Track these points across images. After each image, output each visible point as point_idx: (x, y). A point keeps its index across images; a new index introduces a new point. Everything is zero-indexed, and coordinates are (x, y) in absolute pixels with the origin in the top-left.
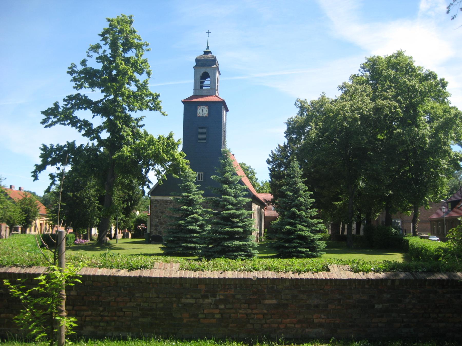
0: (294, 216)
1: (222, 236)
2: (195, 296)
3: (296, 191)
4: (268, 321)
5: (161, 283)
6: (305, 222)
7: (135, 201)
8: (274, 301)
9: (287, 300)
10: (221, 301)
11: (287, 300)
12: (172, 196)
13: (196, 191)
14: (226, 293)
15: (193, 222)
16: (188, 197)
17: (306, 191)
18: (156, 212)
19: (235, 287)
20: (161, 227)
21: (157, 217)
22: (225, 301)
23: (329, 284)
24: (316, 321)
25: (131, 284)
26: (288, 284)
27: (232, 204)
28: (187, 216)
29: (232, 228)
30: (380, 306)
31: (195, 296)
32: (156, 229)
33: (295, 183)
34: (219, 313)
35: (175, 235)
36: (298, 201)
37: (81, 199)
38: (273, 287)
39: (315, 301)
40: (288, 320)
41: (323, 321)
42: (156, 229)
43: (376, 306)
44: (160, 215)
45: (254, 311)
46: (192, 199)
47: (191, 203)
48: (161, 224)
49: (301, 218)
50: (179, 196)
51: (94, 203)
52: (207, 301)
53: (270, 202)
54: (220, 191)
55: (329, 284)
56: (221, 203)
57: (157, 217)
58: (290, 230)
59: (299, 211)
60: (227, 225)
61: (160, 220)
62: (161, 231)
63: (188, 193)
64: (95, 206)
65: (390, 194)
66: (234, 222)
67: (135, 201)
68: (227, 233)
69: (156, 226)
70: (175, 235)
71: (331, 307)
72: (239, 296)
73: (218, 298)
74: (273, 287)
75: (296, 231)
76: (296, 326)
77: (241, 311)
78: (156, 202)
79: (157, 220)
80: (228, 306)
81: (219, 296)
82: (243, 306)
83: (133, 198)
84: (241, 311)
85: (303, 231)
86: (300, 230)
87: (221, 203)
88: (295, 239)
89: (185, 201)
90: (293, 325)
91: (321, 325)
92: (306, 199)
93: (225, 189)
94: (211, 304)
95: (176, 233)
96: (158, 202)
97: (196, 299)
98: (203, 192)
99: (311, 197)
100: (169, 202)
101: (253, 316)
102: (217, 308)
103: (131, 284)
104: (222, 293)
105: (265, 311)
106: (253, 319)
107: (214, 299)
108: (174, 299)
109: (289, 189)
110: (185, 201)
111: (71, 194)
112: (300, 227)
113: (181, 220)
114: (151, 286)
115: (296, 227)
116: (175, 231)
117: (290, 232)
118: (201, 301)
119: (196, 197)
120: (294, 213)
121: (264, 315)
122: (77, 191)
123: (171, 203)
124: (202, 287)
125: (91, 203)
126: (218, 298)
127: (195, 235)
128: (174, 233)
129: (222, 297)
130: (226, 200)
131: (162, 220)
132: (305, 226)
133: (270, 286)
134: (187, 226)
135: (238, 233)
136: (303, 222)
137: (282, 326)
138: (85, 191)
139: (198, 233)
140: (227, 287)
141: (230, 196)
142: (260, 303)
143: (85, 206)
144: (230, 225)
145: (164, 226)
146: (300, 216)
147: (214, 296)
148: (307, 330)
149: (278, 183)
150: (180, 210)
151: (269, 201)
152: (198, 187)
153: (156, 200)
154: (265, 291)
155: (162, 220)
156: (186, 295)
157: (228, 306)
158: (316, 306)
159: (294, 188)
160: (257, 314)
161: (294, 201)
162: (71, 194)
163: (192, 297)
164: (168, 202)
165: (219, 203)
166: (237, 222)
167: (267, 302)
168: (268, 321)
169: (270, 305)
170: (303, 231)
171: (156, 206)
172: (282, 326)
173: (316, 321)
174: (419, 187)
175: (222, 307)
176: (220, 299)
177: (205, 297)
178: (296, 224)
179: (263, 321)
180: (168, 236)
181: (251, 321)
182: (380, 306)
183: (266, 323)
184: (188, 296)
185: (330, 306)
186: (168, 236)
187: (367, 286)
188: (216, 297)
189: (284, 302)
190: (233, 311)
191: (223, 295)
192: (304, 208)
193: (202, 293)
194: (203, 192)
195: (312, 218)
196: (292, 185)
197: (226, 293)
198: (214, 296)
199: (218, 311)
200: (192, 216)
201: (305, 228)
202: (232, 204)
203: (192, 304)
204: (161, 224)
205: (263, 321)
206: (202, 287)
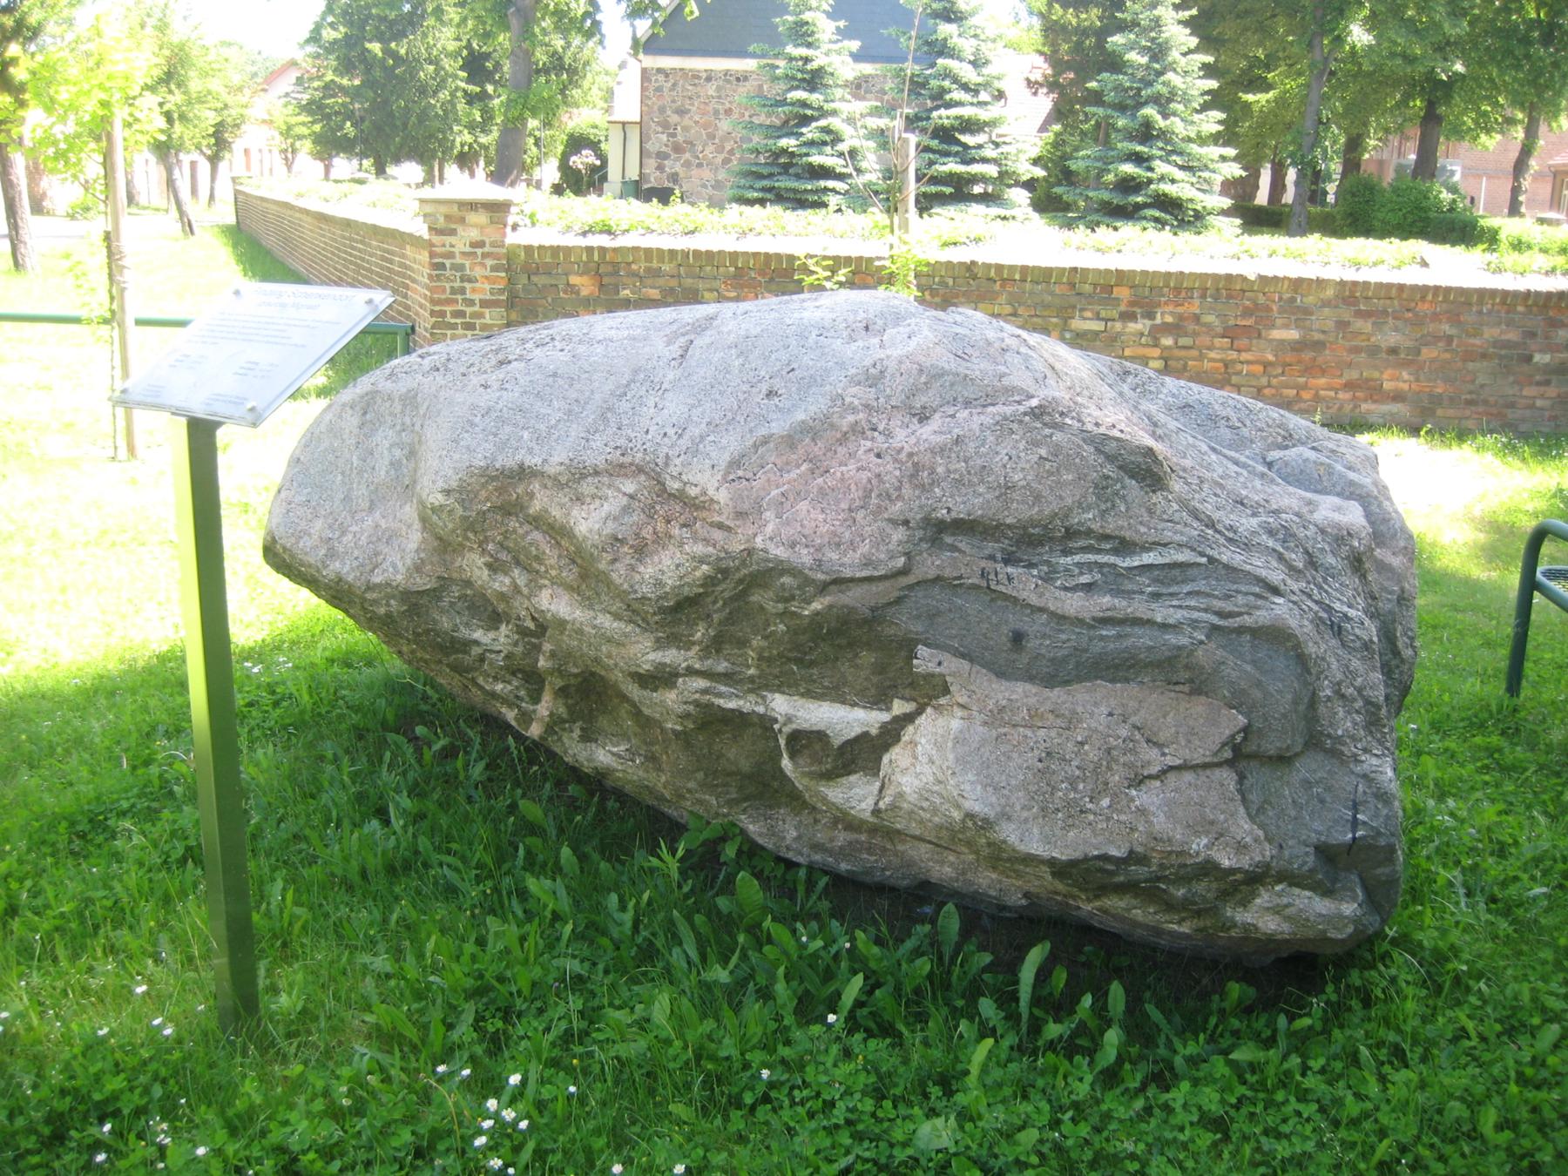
0: (1146, 133)
1: (933, 189)
2: (1103, 314)
3: (1158, 52)
4: (1274, 381)
5: (1023, 280)
6: (1181, 154)
7: (572, 71)
8: (1293, 334)
9: (1324, 332)
10: (1166, 328)
11: (1324, 332)
12: (753, 55)
13: (831, 42)
14: (1180, 310)
15: (825, 143)
16: (807, 60)
17: (1190, 52)
18: (662, 110)
19: (1203, 296)
20: (677, 159)
21: (665, 125)
22: (1174, 329)
23: (1430, 297)
24: (1387, 386)
25: (951, 282)
26: (1330, 293)
27: (965, 87)
28: (805, 120)
29: (965, 162)
30: (1547, 358)
31: (1103, 314)
32: (660, 168)
33: (1157, 23)
34: (1161, 358)
35: (766, 183)
36: (1164, 83)
37: (412, 64)
38: (1293, 300)
39: (1389, 338)
40: (1322, 381)
41: (1405, 387)
42: (660, 168)
43: (1537, 358)
44: (674, 118)
45: (1245, 356)
46: (821, 69)
47: (814, 80)
48: (678, 149)
49: (1168, 142)
50: (776, 56)
51: (456, 77)
52: (1133, 327)
53: (1041, 85)
54: (927, 43)
55: (1430, 297)
56: (934, 83)
57: (665, 125)
58: (1134, 179)
59: (1165, 116)
60: (947, 154)
61: (674, 135)
62: (676, 174)
63: (809, 45)
64: (457, 89)
65: (1456, 73)
66: (966, 147)
67: (572, 71)
68: (950, 179)
69: (662, 156)
70: (766, 183)
71: (1427, 353)
72: (1210, 318)
73: (1158, 321)
74: (1293, 300)
75: (1150, 181)
76: (1341, 395)
77: (1212, 355)
78: (661, 78)
79: (664, 138)
80: (1183, 341)
81: (1164, 316)
82: (1217, 340)
83: (567, 61)
84: (1212, 355)
85: (1173, 181)
86: (1162, 179)
87: (934, 83)
88: (1146, 206)
89: (799, 76)
90: (1332, 394)
91: (1398, 397)
92: (1189, 79)
93: (945, 39)
94: (1142, 334)
95: (771, 176)
96: (667, 75)
97: (1107, 320)
98: (855, 45)
99: (1208, 71)
100: (704, 75)
101: (1239, 367)
102: (1156, 346)
103: (951, 282)
104: (1170, 308)
105: (1271, 358)
106: (1239, 373)
107: (1148, 323)
108: (1054, 320)
109: (1136, 42)
110: (799, 76)
111: (375, 47)
112: (1161, 167)
113: (789, 135)
114: (997, 287)
115: (1151, 169)
116: (765, 171)
117: (1128, 185)
118: (1118, 326)
119: (834, 58)
120: (1147, 124)
121: (1266, 365)
122: (399, 35)
123: (709, 79)
124: (1123, 293)
125: (444, 80)
126: (1158, 321)
127: (831, 184)
128: (761, 177)
129: (1169, 319)
130: (947, 74)
131: (680, 138)
132: (1182, 168)
133: (1286, 296)
134: (807, 155)
135: (983, 179)
136: (1173, 152)
137: (1306, 395)
138: (425, 35)
139: (841, 177)
140: (1183, 294)
141: (961, 60)
142: (1259, 336)
143: (423, 91)
144: (957, 153)
145: (687, 155)
146: (1164, 135)
147: (1150, 315)
148: (1364, 407)
149: (1074, 21)
150: (783, 103)
151: (1036, 82)
152: (838, 28)
153: (659, 70)
154: (1275, 308)
155: (680, 138)
156: (1082, 310)
157: (1183, 341)
158: (1393, 351)
159: (1153, 40)
160: (1248, 362)
161: (1150, 84)
162: (375, 47)
163: (1098, 317)
164: (699, 77)
165: (924, 85)
166: (980, 147)
167: (1277, 334)
168: (1274, 381)
169: (1282, 341)
170: (1173, 181)
171: (659, 89)
172: (1306, 395)
173: (1387, 386)
174: (1557, 50)
175: (1167, 341)
176: (1164, 324)
177: (1128, 316)
178: (1150, 158)
179: (1264, 381)
180: (743, 187)
181: (1234, 379)
182: (1547, 358)
183: (1269, 386)
184: (1088, 314)
185: (1424, 350)
186: (743, 187)
187: (1520, 309)
188: (1154, 318)
189: (1317, 336)
190: (1194, 353)
191: (1171, 313)
192: (1180, 107)
193: (1123, 308)
194: (855, 45)
195: (1202, 140)
196: (1145, 30)
197: (1180, 310)
198: (1150, 315)
199: (1156, 352)
200: (822, 123)
201: (1179, 174)
202: (965, 87)
203: (1097, 333)
204: (678, 149)
205: (1264, 381)
206: (1123, 293)
